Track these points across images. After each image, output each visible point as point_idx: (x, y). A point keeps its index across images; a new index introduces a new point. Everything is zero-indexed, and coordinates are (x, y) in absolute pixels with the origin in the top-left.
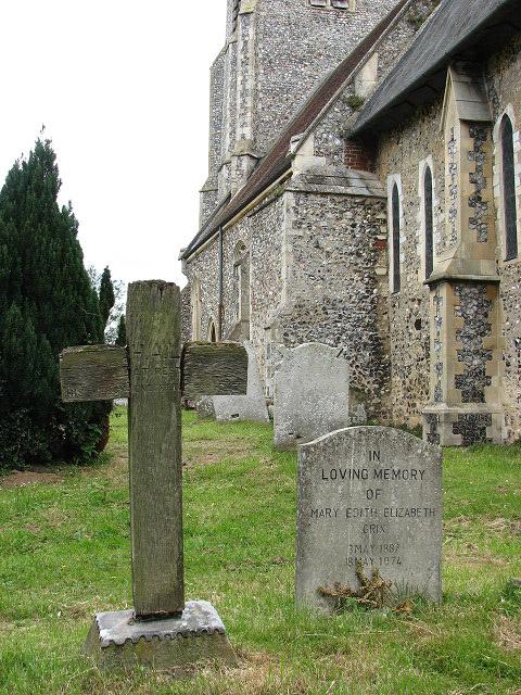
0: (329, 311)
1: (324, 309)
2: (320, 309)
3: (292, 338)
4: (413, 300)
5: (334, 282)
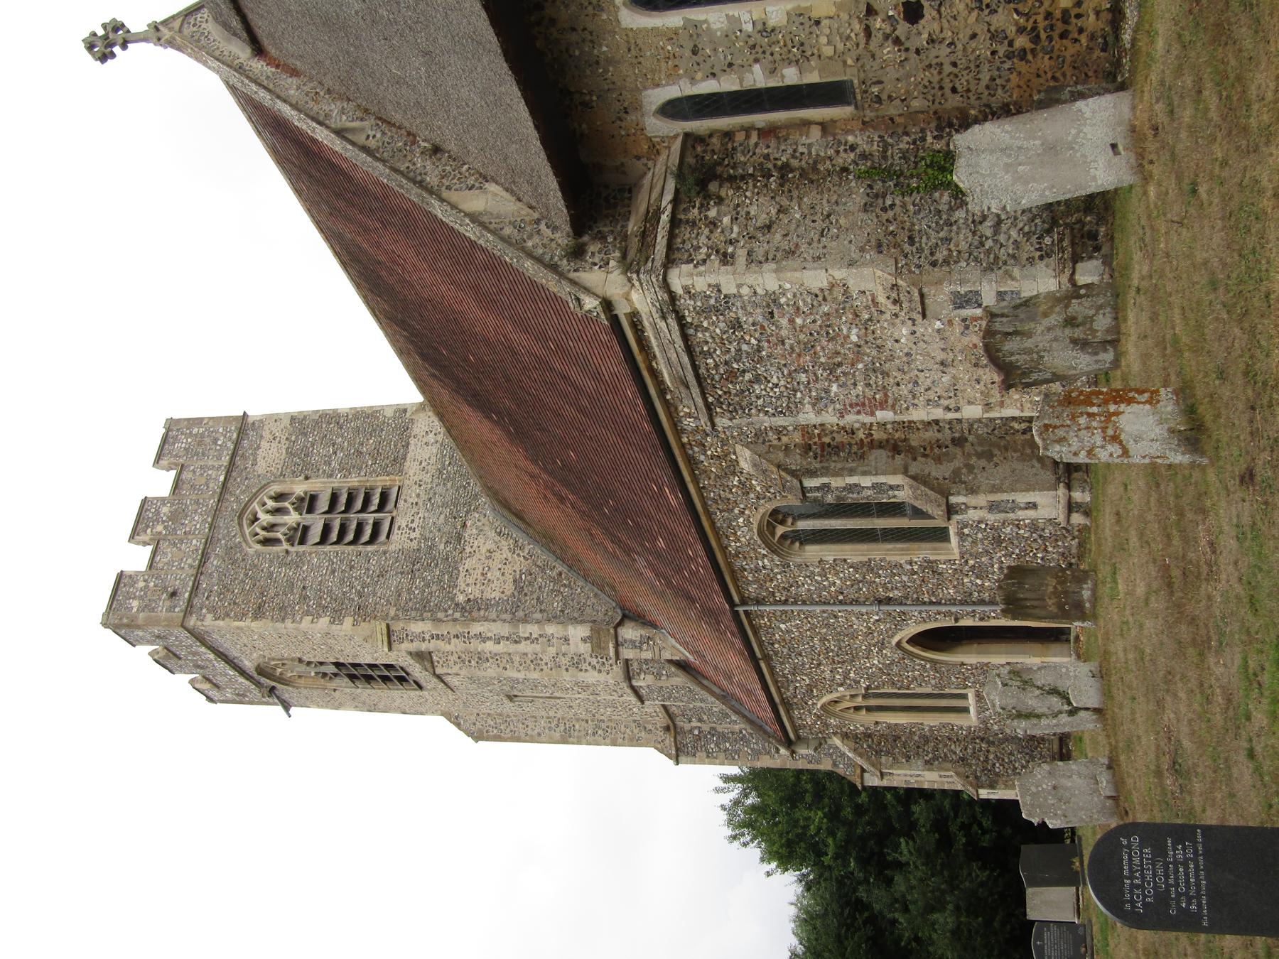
0: (888, 202)
1: (884, 209)
2: (885, 216)
3: (940, 256)
4: (868, 32)
5: (834, 198)
